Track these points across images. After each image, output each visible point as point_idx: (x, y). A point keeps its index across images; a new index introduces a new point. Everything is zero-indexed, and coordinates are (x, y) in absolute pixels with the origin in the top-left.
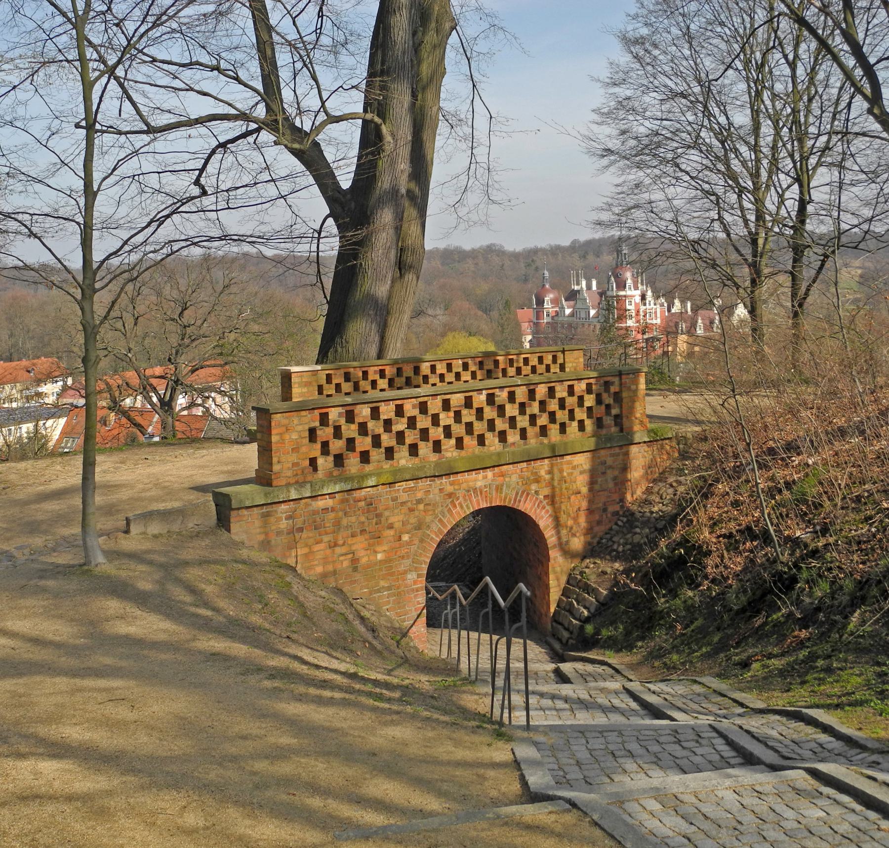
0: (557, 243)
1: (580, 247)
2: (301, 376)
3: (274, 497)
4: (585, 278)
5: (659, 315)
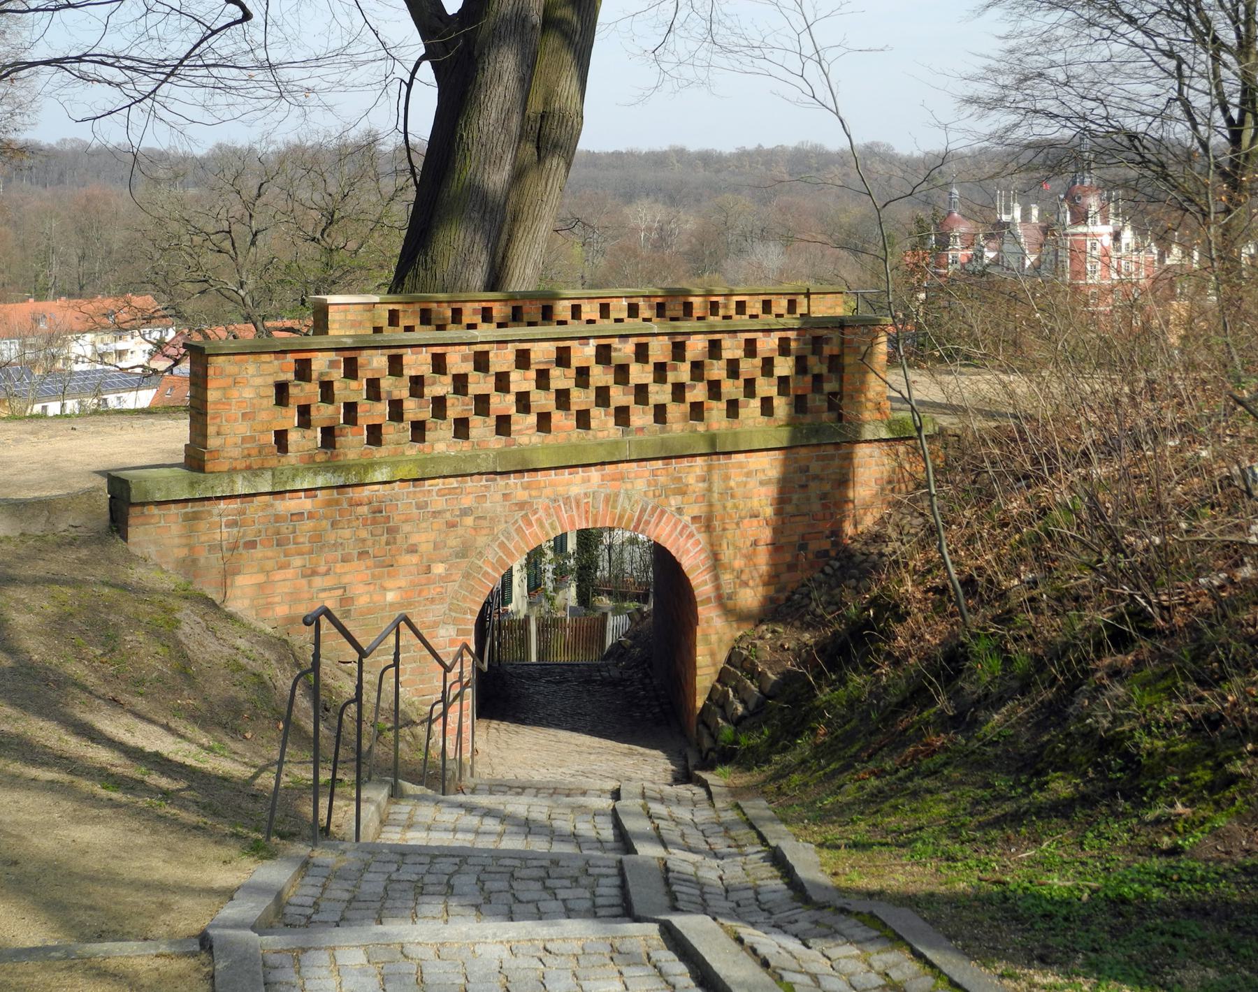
2: (345, 311)
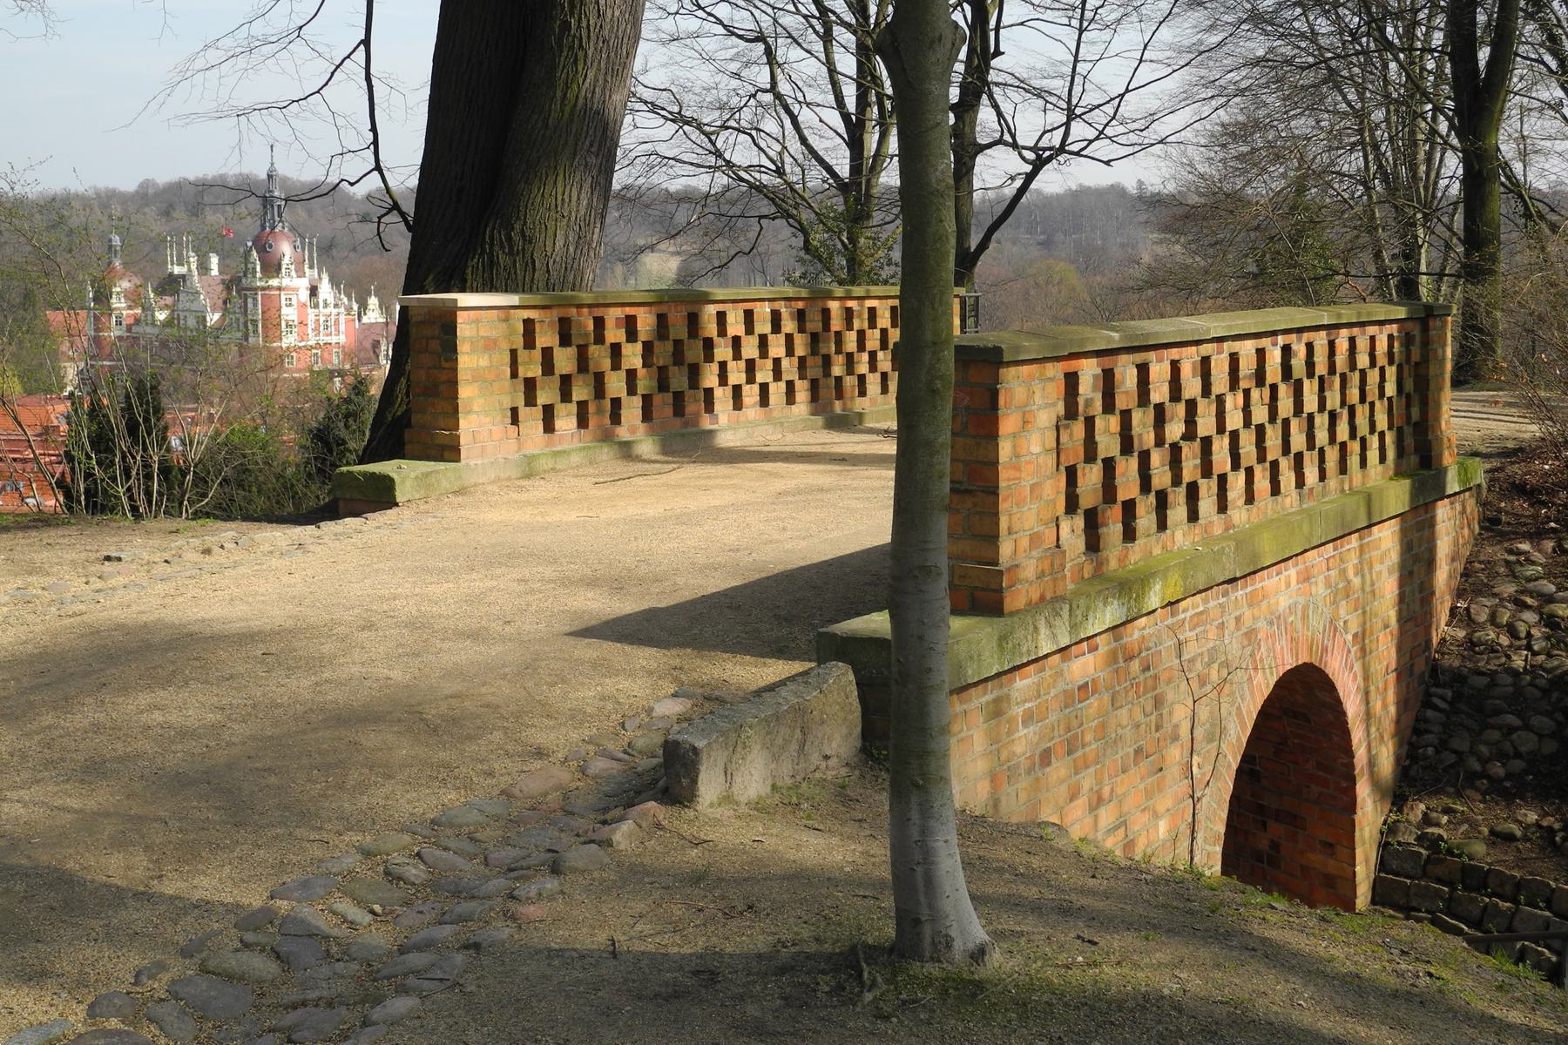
0: (111, 186)
1: (156, 195)
2: (477, 321)
3: (1021, 655)
4: (197, 250)
5: (342, 327)
